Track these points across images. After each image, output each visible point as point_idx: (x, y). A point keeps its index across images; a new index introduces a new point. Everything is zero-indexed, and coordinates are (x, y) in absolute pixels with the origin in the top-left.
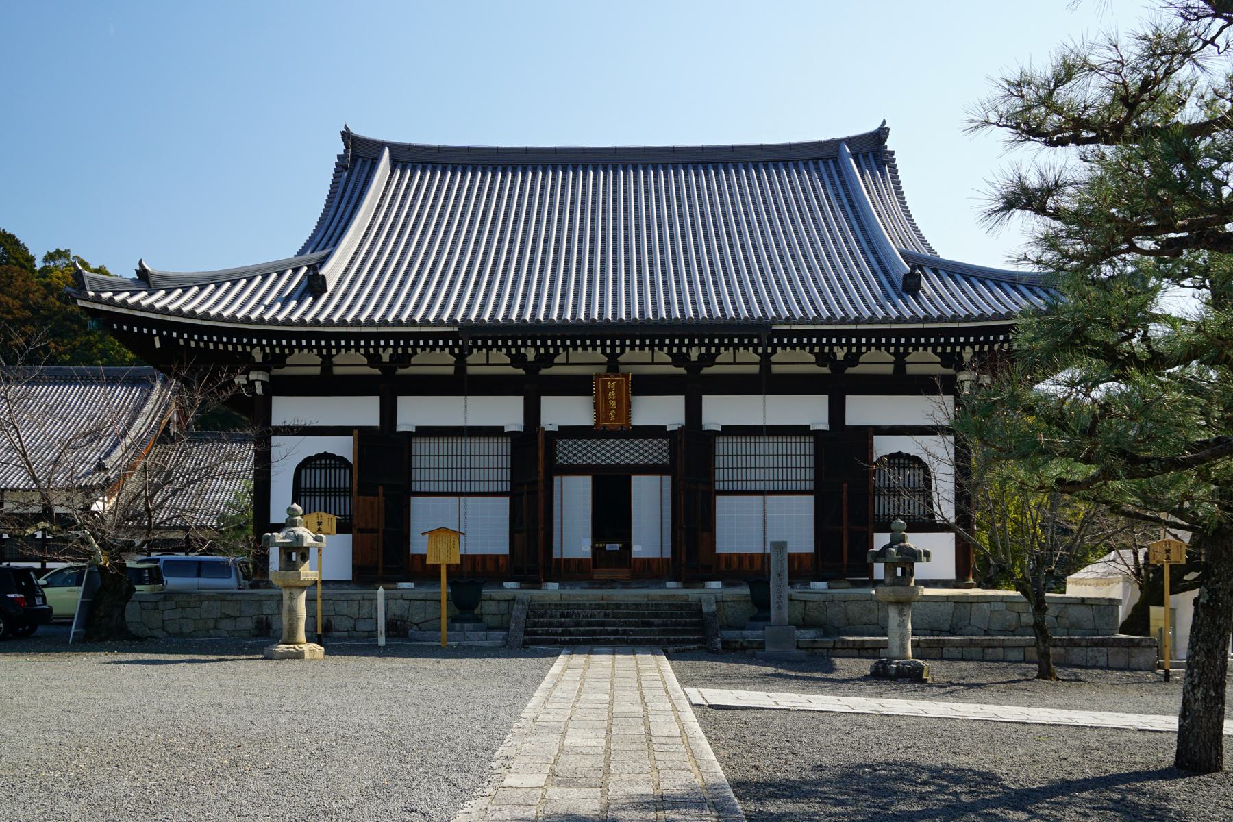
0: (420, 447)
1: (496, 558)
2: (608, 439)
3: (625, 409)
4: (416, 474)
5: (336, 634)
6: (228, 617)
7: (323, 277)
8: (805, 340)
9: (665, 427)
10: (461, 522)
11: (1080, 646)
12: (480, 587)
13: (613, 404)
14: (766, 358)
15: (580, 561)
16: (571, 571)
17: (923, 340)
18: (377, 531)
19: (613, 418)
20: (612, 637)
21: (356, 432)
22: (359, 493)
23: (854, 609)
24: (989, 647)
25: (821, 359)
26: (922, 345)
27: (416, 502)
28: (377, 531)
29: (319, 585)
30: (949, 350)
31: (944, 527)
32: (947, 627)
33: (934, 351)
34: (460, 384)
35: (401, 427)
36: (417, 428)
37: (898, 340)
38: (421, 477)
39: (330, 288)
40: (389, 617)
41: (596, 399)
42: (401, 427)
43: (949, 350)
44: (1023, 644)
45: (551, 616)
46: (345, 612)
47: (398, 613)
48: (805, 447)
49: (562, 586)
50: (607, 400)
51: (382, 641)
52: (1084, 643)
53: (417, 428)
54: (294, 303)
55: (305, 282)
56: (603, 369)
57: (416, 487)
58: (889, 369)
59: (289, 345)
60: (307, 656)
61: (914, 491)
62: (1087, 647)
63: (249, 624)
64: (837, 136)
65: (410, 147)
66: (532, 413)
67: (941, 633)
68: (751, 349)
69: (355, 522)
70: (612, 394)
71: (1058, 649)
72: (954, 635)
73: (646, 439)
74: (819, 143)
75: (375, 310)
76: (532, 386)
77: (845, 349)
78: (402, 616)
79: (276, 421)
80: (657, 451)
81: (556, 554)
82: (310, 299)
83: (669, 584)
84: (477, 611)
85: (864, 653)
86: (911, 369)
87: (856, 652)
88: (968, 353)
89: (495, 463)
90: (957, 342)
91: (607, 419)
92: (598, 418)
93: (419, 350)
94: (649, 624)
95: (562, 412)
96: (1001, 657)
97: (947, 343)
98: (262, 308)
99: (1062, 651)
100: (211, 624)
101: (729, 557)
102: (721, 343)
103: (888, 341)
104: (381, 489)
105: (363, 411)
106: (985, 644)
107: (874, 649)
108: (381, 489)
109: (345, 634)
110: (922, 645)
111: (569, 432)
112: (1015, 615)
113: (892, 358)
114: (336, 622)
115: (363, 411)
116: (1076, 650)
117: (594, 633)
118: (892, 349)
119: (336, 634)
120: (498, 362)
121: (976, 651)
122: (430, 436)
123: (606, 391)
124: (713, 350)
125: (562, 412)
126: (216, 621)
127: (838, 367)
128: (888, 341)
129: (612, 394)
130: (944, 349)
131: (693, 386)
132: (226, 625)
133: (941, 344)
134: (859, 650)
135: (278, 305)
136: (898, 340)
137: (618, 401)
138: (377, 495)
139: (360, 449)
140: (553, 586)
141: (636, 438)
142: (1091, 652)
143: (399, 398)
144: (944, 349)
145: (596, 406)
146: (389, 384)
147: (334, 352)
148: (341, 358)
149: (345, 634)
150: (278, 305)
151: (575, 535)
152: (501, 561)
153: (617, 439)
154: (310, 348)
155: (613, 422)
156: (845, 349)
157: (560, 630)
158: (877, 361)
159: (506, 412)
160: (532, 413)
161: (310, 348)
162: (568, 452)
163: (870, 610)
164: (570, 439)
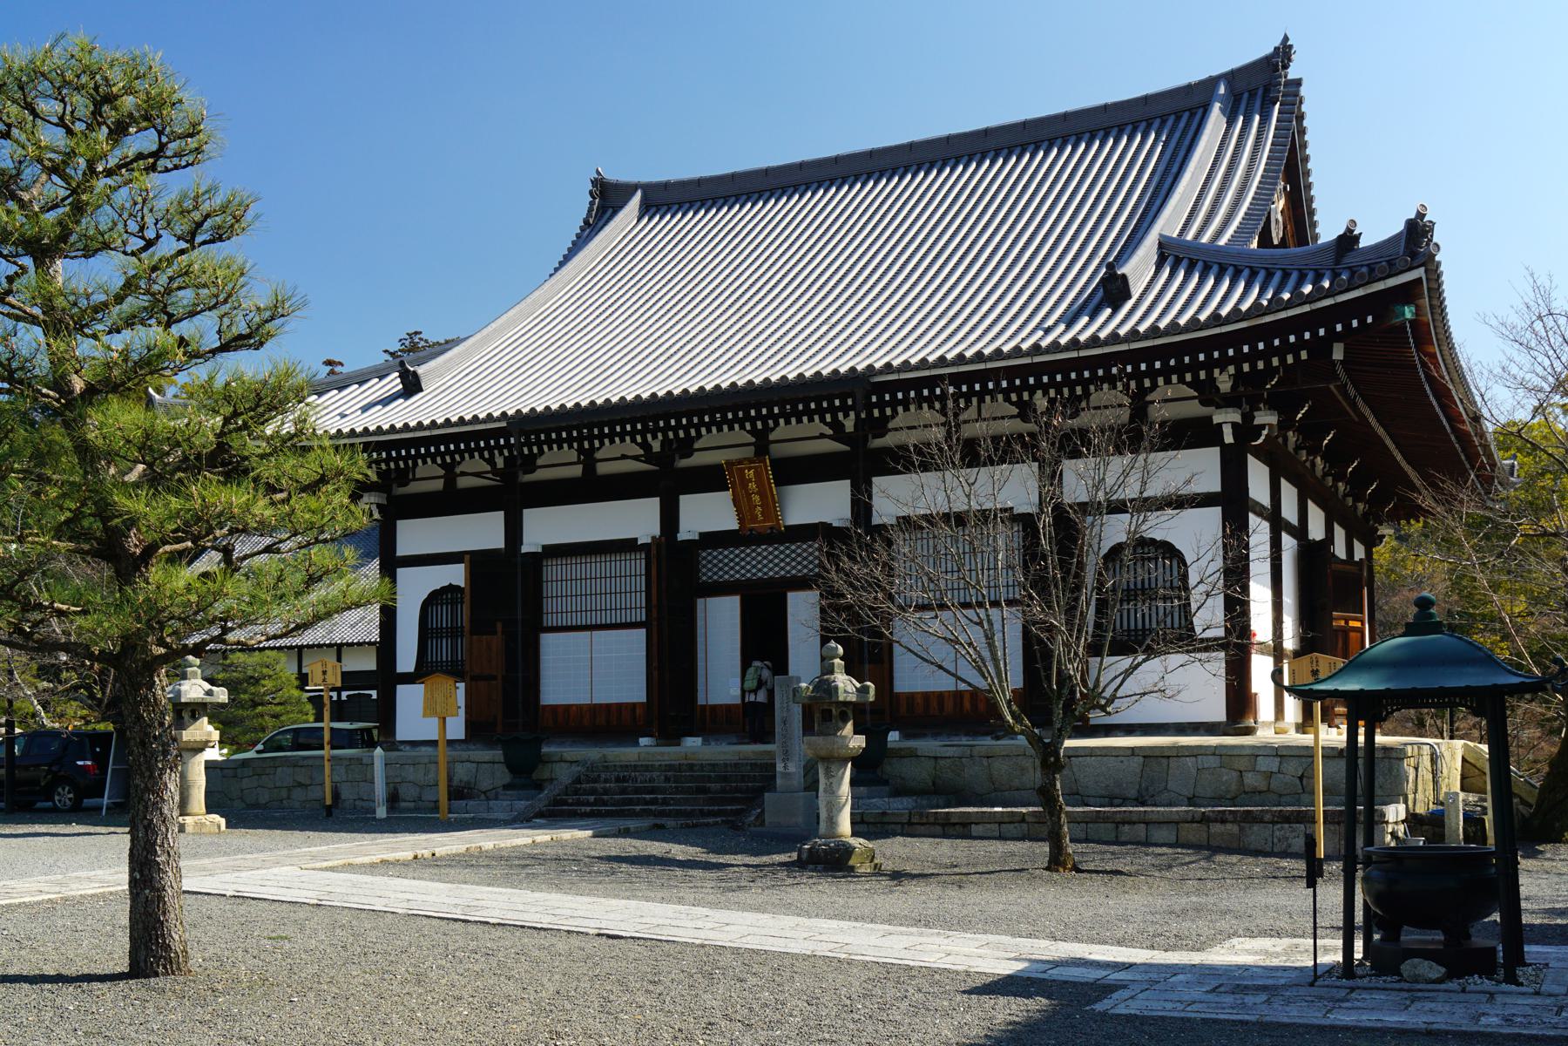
0: (553, 571)
1: (633, 706)
3: (772, 507)
4: (549, 605)
5: (403, 804)
6: (300, 785)
7: (1124, 277)
10: (595, 665)
11: (1262, 821)
12: (539, 742)
13: (756, 498)
15: (728, 708)
16: (717, 722)
17: (673, 422)
18: (494, 678)
19: (760, 517)
21: (467, 557)
22: (472, 633)
23: (1001, 768)
24: (1124, 823)
27: (548, 641)
28: (494, 678)
29: (441, 745)
31: (1209, 646)
32: (1133, 793)
33: (1007, 399)
35: (682, 536)
36: (544, 547)
38: (555, 607)
39: (1136, 293)
40: (455, 783)
41: (734, 494)
42: (682, 536)
44: (1176, 818)
45: (606, 781)
46: (411, 778)
48: (637, 564)
49: (706, 742)
50: (749, 495)
51: (381, 812)
52: (1268, 817)
54: (1085, 319)
55: (1100, 293)
56: (749, 452)
57: (549, 620)
58: (577, 471)
59: (771, 414)
61: (439, 633)
62: (1273, 823)
64: (1214, 74)
65: (666, 186)
66: (670, 518)
67: (1125, 801)
68: (1000, 397)
69: (467, 668)
70: (752, 486)
71: (1229, 826)
72: (1143, 805)
74: (1189, 86)
75: (1081, 332)
76: (667, 482)
78: (468, 783)
79: (402, 551)
81: (701, 701)
82: (1109, 311)
84: (534, 776)
85: (951, 831)
86: (603, 469)
87: (938, 829)
88: (1224, 383)
89: (628, 585)
90: (690, 424)
91: (754, 519)
92: (741, 520)
94: (704, 791)
95: (707, 513)
96: (1143, 839)
98: (1041, 333)
99: (1234, 828)
100: (284, 793)
101: (911, 696)
102: (702, 423)
104: (499, 626)
105: (482, 531)
106: (1118, 818)
107: (964, 825)
108: (499, 626)
109: (412, 805)
110: (1029, 819)
111: (712, 540)
112: (1235, 774)
113: (442, 472)
114: (403, 791)
115: (482, 531)
116: (1256, 828)
117: (630, 802)
119: (403, 804)
121: (1105, 830)
122: (556, 557)
123: (744, 482)
125: (707, 513)
126: (289, 789)
129: (752, 486)
131: (860, 464)
132: (298, 794)
133: (639, 432)
134: (943, 825)
135: (1062, 327)
137: (762, 494)
138: (495, 633)
139: (472, 575)
140: (693, 743)
141: (793, 542)
142: (1280, 831)
143: (682, 497)
144: (754, 425)
145: (736, 502)
146: (512, 495)
147: (888, 411)
149: (412, 805)
150: (1062, 327)
151: (722, 676)
152: (638, 711)
153: (770, 545)
155: (761, 524)
157: (592, 798)
158: (559, 463)
159: (637, 519)
160: (670, 518)
162: (715, 566)
163: (1023, 769)
164: (715, 549)
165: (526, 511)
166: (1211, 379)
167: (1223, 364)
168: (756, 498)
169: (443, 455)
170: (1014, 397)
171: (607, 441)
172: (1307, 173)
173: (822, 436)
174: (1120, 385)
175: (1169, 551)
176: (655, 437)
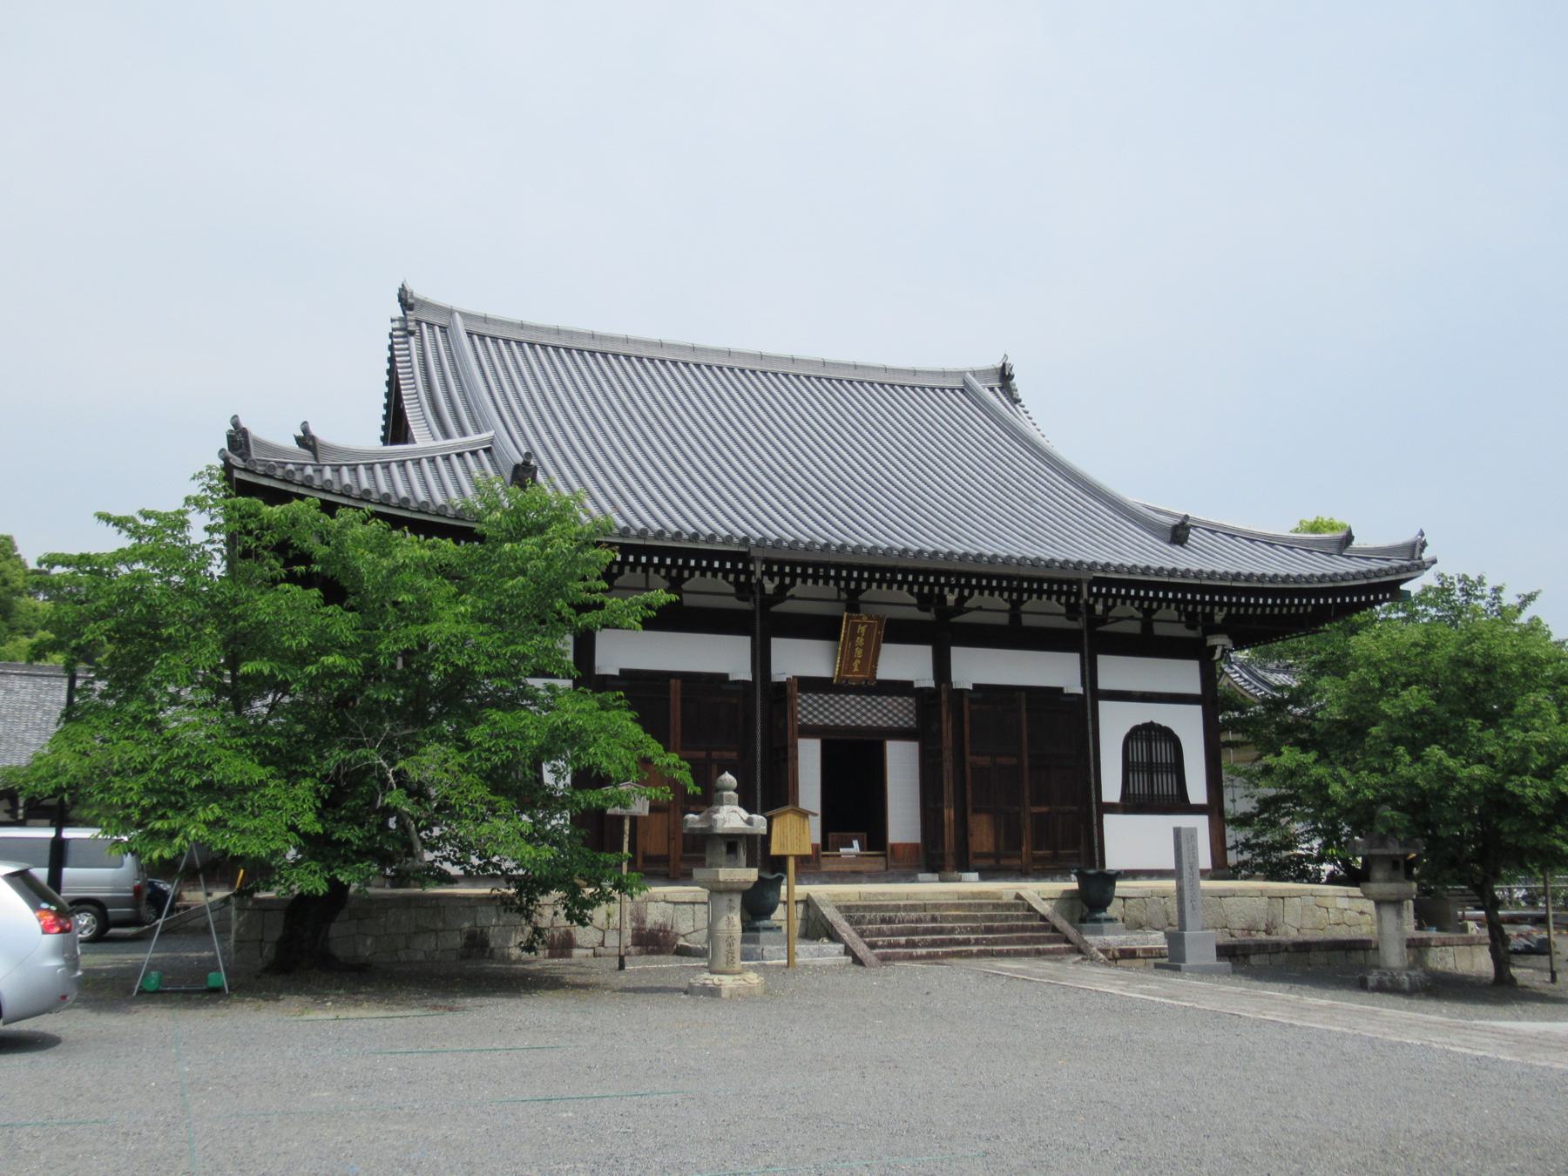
2: (847, 694)
3: (872, 659)
8: (716, 564)
9: (726, 676)
13: (859, 652)
14: (1016, 605)
17: (656, 560)
20: (975, 949)
25: (924, 602)
26: (1045, 592)
30: (926, 589)
31: (1197, 810)
33: (910, 591)
34: (1014, 635)
36: (622, 671)
37: (861, 574)
43: (926, 589)
47: (661, 920)
50: (854, 647)
53: (622, 671)
58: (1003, 619)
60: (725, 994)
63: (458, 941)
66: (942, 667)
70: (860, 641)
73: (816, 693)
76: (762, 621)
77: (777, 580)
80: (898, 712)
83: (921, 876)
86: (1027, 620)
90: (1212, 601)
91: (849, 669)
93: (627, 569)
95: (798, 659)
97: (926, 582)
103: (838, 573)
111: (809, 684)
118: (1063, 599)
120: (712, 590)
123: (854, 634)
124: (1155, 605)
127: (1094, 621)
128: (838, 573)
129: (860, 641)
130: (921, 589)
136: (861, 574)
137: (866, 649)
144: (921, 589)
147: (864, 585)
148: (1032, 604)
154: (827, 579)
155: (856, 674)
156: (777, 580)
160: (942, 667)
161: (827, 579)
162: (809, 709)
165: (773, 640)
166: (1212, 613)
167: (1221, 604)
168: (859, 652)
169: (1187, 602)
170: (916, 589)
171: (874, 585)
172: (385, 417)
173: (1132, 618)
174: (1006, 595)
175: (1168, 736)
176: (952, 591)
